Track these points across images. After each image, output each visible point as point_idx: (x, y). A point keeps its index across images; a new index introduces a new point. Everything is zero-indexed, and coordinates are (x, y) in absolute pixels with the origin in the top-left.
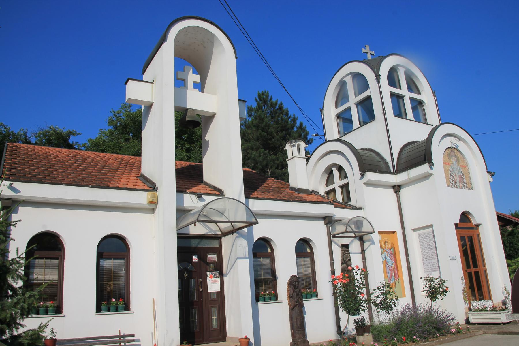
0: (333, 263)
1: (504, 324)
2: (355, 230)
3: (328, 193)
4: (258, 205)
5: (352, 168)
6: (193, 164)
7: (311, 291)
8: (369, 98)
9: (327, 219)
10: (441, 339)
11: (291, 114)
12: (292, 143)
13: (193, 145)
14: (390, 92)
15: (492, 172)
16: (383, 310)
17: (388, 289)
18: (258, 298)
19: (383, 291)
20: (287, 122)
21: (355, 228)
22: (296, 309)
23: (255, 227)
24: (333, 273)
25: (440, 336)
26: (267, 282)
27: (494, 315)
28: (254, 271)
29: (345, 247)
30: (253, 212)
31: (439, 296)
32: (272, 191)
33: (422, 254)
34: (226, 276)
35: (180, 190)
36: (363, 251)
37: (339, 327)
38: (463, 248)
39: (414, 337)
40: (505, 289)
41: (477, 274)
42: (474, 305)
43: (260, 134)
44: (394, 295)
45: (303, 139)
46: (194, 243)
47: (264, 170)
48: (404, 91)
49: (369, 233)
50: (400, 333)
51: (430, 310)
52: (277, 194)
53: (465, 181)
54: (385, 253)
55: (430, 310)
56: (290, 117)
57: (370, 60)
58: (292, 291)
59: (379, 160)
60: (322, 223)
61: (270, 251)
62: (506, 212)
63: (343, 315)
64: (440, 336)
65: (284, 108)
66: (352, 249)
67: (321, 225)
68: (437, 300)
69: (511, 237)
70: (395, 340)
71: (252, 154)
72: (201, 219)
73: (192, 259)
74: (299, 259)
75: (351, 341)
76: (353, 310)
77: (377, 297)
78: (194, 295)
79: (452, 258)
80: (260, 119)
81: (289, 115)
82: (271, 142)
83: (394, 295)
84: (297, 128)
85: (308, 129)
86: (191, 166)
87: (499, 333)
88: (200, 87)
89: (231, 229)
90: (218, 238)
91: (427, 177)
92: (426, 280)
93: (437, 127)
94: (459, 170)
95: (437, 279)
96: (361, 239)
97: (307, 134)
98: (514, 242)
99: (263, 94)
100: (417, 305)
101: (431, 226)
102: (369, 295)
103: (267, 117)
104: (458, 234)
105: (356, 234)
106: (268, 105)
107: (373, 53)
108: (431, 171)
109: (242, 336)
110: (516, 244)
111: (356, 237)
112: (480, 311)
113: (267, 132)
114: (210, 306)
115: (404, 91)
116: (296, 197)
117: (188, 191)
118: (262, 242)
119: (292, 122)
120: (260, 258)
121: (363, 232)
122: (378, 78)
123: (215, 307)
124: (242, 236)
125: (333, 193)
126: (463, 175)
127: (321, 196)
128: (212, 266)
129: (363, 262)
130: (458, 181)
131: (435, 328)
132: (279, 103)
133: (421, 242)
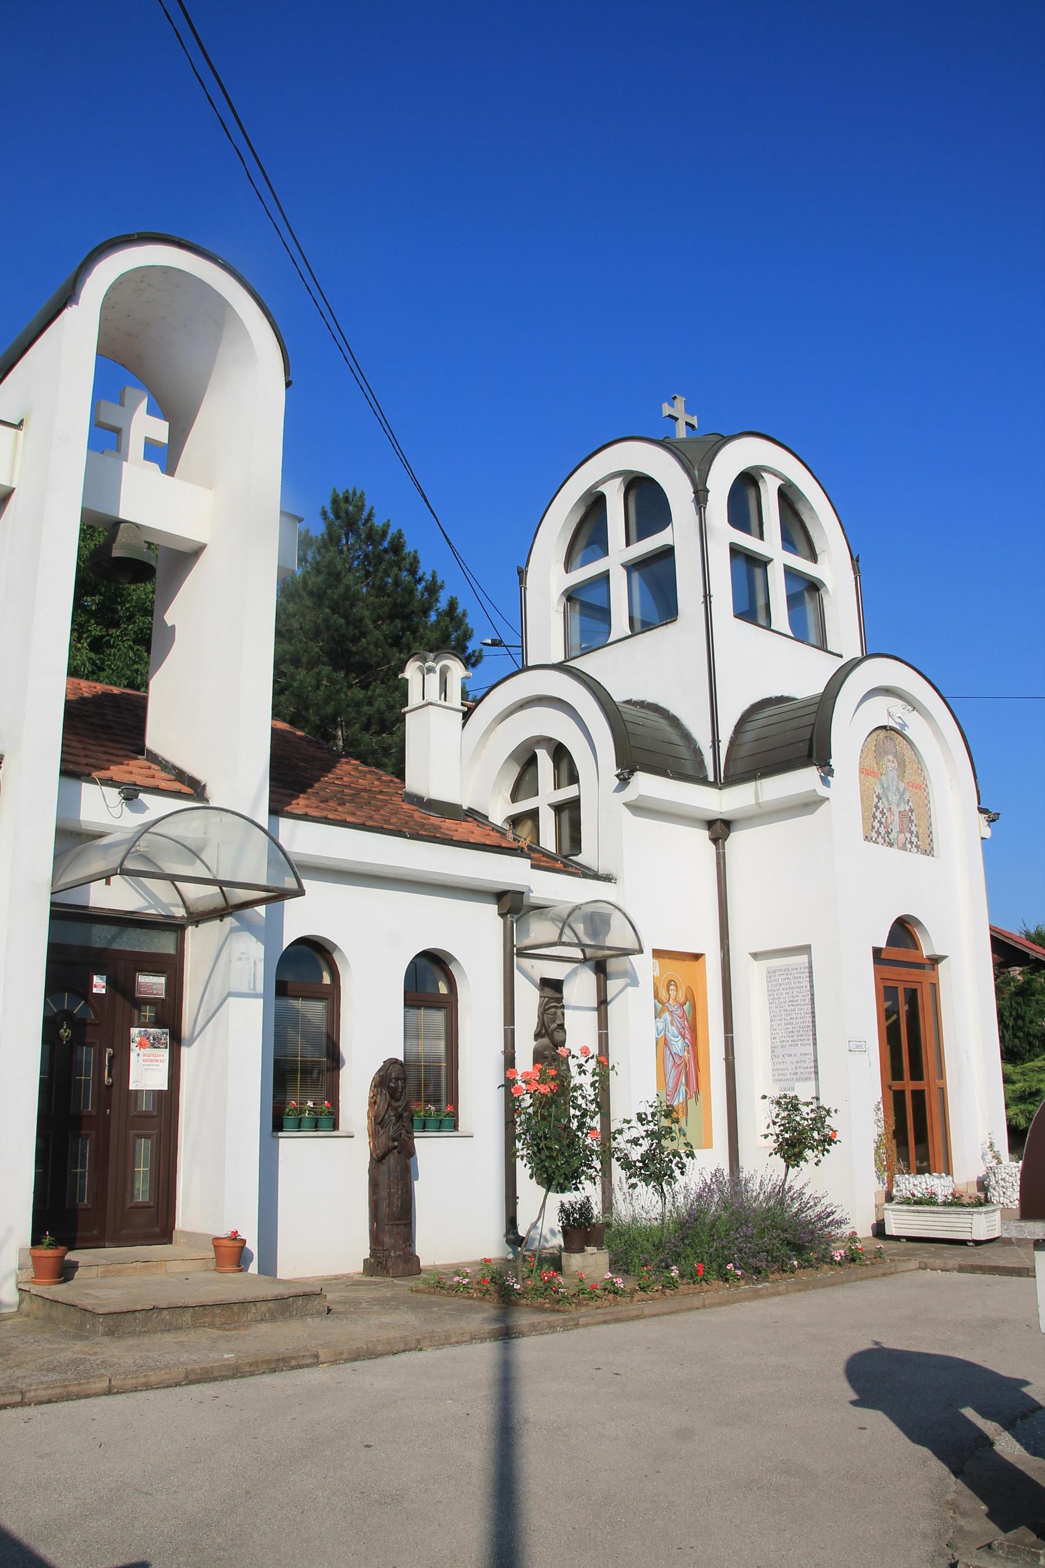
0: (513, 1030)
1: (978, 1243)
2: (587, 941)
3: (515, 821)
4: (305, 838)
5: (597, 757)
6: (116, 690)
7: (438, 1110)
8: (667, 553)
9: (507, 899)
10: (804, 1275)
11: (425, 569)
12: (424, 660)
13: (112, 631)
14: (731, 544)
15: (993, 810)
16: (646, 1180)
17: (665, 1122)
18: (279, 1120)
19: (651, 1127)
20: (411, 592)
21: (586, 934)
22: (392, 1160)
23: (290, 904)
24: (510, 1061)
25: (800, 1267)
26: (311, 1072)
27: (953, 1219)
28: (277, 1035)
29: (552, 987)
30: (291, 858)
31: (808, 1153)
32: (352, 801)
33: (772, 1029)
34: (189, 1045)
35: (74, 769)
36: (603, 1002)
37: (511, 1222)
38: (888, 1018)
39: (730, 1266)
40: (991, 1145)
41: (919, 1097)
42: (902, 1187)
43: (326, 620)
44: (682, 1140)
45: (454, 648)
46: (100, 936)
47: (334, 733)
48: (770, 545)
49: (625, 952)
50: (689, 1251)
51: (781, 1193)
52: (367, 810)
53: (914, 828)
54: (666, 1015)
55: (781, 1193)
56: (421, 579)
57: (682, 441)
58: (382, 1106)
59: (677, 739)
60: (492, 909)
61: (327, 979)
62: (1015, 929)
63: (529, 1189)
64: (800, 1267)
65: (406, 551)
66: (570, 994)
67: (488, 917)
68: (802, 1163)
69: (1020, 999)
70: (675, 1272)
71: (293, 677)
72: (130, 865)
73: (90, 984)
74: (413, 1012)
75: (545, 1267)
76: (555, 1175)
77: (632, 1142)
78: (86, 1097)
79: (857, 1048)
80: (330, 574)
81: (420, 573)
82: (354, 649)
83: (682, 1140)
84: (439, 615)
85: (470, 622)
86: (106, 695)
87: (961, 1269)
88: (166, 457)
89: (219, 902)
90: (176, 927)
91: (810, 804)
92: (778, 1103)
93: (853, 665)
94: (901, 797)
95: (807, 1104)
96: (600, 968)
97: (467, 635)
98: (1029, 1015)
99: (346, 500)
100: (744, 1175)
101: (806, 949)
102: (608, 1135)
103: (350, 570)
104: (879, 979)
105: (588, 951)
106: (358, 536)
107: (694, 421)
108: (822, 791)
109: (224, 1232)
110: (1031, 1022)
111: (585, 960)
112: (916, 1203)
113: (345, 616)
114: (132, 1132)
115: (770, 545)
116: (423, 825)
117: (96, 775)
118: (305, 948)
119: (426, 595)
120: (296, 997)
121: (609, 948)
122: (701, 497)
123: (146, 1137)
124: (249, 927)
125: (529, 824)
126: (911, 811)
127: (495, 829)
128: (148, 1013)
129: (600, 1035)
130: (895, 827)
131: (789, 1243)
132: (392, 531)
133: (771, 993)
